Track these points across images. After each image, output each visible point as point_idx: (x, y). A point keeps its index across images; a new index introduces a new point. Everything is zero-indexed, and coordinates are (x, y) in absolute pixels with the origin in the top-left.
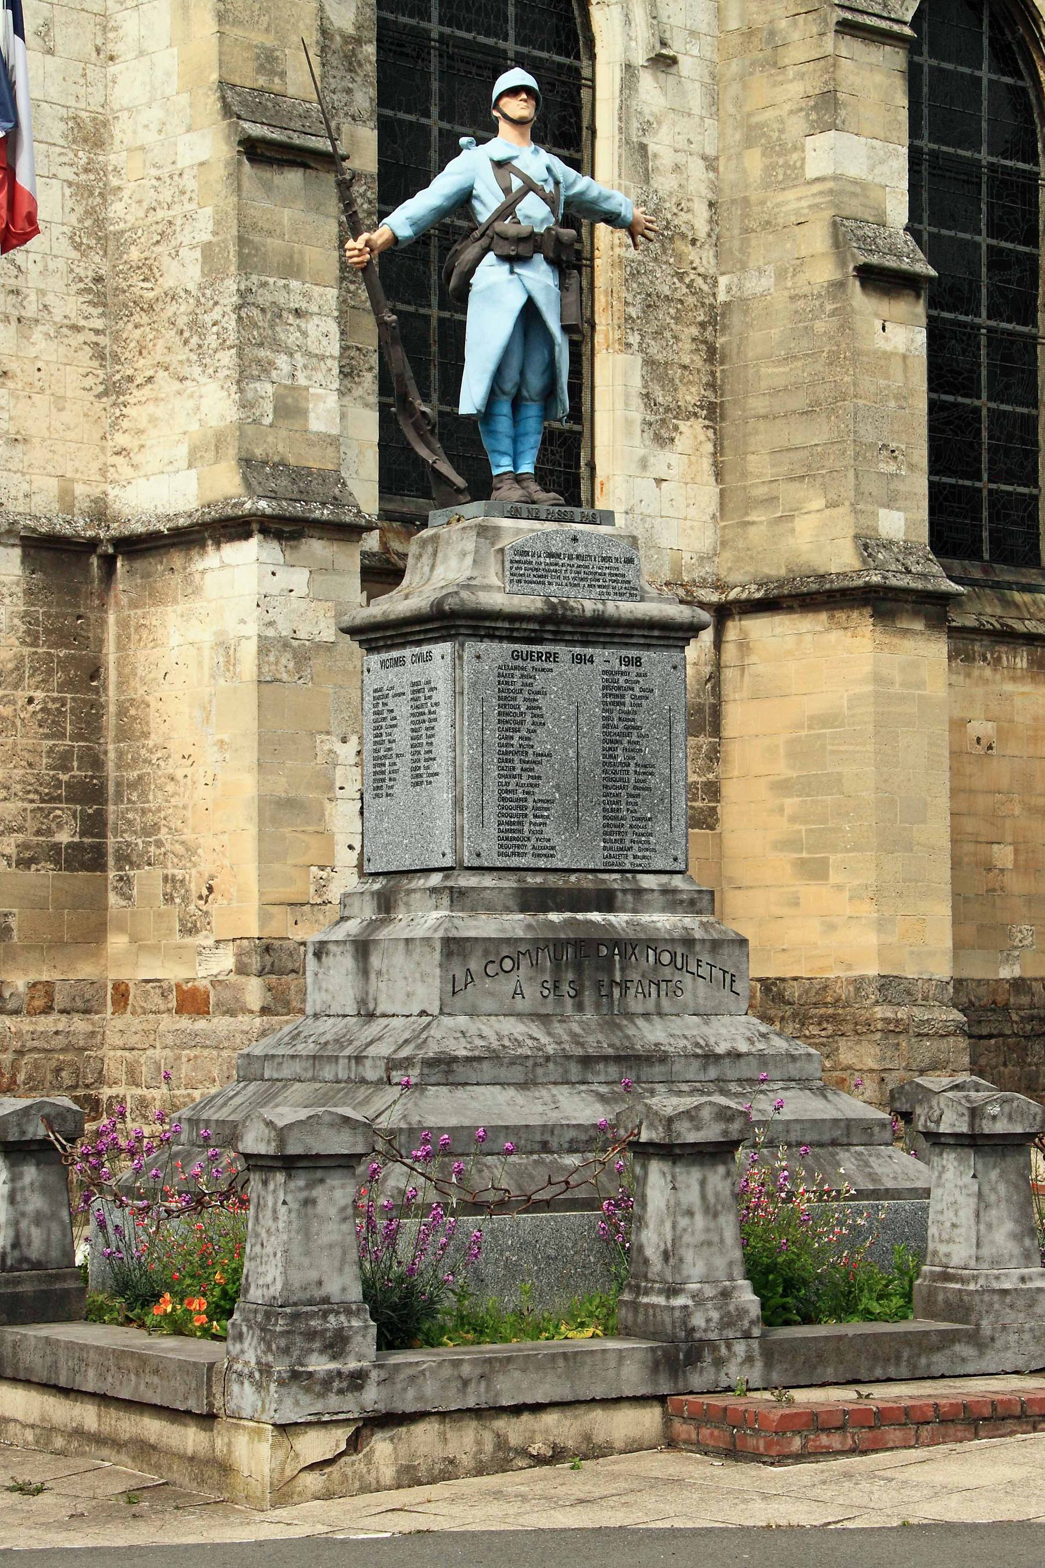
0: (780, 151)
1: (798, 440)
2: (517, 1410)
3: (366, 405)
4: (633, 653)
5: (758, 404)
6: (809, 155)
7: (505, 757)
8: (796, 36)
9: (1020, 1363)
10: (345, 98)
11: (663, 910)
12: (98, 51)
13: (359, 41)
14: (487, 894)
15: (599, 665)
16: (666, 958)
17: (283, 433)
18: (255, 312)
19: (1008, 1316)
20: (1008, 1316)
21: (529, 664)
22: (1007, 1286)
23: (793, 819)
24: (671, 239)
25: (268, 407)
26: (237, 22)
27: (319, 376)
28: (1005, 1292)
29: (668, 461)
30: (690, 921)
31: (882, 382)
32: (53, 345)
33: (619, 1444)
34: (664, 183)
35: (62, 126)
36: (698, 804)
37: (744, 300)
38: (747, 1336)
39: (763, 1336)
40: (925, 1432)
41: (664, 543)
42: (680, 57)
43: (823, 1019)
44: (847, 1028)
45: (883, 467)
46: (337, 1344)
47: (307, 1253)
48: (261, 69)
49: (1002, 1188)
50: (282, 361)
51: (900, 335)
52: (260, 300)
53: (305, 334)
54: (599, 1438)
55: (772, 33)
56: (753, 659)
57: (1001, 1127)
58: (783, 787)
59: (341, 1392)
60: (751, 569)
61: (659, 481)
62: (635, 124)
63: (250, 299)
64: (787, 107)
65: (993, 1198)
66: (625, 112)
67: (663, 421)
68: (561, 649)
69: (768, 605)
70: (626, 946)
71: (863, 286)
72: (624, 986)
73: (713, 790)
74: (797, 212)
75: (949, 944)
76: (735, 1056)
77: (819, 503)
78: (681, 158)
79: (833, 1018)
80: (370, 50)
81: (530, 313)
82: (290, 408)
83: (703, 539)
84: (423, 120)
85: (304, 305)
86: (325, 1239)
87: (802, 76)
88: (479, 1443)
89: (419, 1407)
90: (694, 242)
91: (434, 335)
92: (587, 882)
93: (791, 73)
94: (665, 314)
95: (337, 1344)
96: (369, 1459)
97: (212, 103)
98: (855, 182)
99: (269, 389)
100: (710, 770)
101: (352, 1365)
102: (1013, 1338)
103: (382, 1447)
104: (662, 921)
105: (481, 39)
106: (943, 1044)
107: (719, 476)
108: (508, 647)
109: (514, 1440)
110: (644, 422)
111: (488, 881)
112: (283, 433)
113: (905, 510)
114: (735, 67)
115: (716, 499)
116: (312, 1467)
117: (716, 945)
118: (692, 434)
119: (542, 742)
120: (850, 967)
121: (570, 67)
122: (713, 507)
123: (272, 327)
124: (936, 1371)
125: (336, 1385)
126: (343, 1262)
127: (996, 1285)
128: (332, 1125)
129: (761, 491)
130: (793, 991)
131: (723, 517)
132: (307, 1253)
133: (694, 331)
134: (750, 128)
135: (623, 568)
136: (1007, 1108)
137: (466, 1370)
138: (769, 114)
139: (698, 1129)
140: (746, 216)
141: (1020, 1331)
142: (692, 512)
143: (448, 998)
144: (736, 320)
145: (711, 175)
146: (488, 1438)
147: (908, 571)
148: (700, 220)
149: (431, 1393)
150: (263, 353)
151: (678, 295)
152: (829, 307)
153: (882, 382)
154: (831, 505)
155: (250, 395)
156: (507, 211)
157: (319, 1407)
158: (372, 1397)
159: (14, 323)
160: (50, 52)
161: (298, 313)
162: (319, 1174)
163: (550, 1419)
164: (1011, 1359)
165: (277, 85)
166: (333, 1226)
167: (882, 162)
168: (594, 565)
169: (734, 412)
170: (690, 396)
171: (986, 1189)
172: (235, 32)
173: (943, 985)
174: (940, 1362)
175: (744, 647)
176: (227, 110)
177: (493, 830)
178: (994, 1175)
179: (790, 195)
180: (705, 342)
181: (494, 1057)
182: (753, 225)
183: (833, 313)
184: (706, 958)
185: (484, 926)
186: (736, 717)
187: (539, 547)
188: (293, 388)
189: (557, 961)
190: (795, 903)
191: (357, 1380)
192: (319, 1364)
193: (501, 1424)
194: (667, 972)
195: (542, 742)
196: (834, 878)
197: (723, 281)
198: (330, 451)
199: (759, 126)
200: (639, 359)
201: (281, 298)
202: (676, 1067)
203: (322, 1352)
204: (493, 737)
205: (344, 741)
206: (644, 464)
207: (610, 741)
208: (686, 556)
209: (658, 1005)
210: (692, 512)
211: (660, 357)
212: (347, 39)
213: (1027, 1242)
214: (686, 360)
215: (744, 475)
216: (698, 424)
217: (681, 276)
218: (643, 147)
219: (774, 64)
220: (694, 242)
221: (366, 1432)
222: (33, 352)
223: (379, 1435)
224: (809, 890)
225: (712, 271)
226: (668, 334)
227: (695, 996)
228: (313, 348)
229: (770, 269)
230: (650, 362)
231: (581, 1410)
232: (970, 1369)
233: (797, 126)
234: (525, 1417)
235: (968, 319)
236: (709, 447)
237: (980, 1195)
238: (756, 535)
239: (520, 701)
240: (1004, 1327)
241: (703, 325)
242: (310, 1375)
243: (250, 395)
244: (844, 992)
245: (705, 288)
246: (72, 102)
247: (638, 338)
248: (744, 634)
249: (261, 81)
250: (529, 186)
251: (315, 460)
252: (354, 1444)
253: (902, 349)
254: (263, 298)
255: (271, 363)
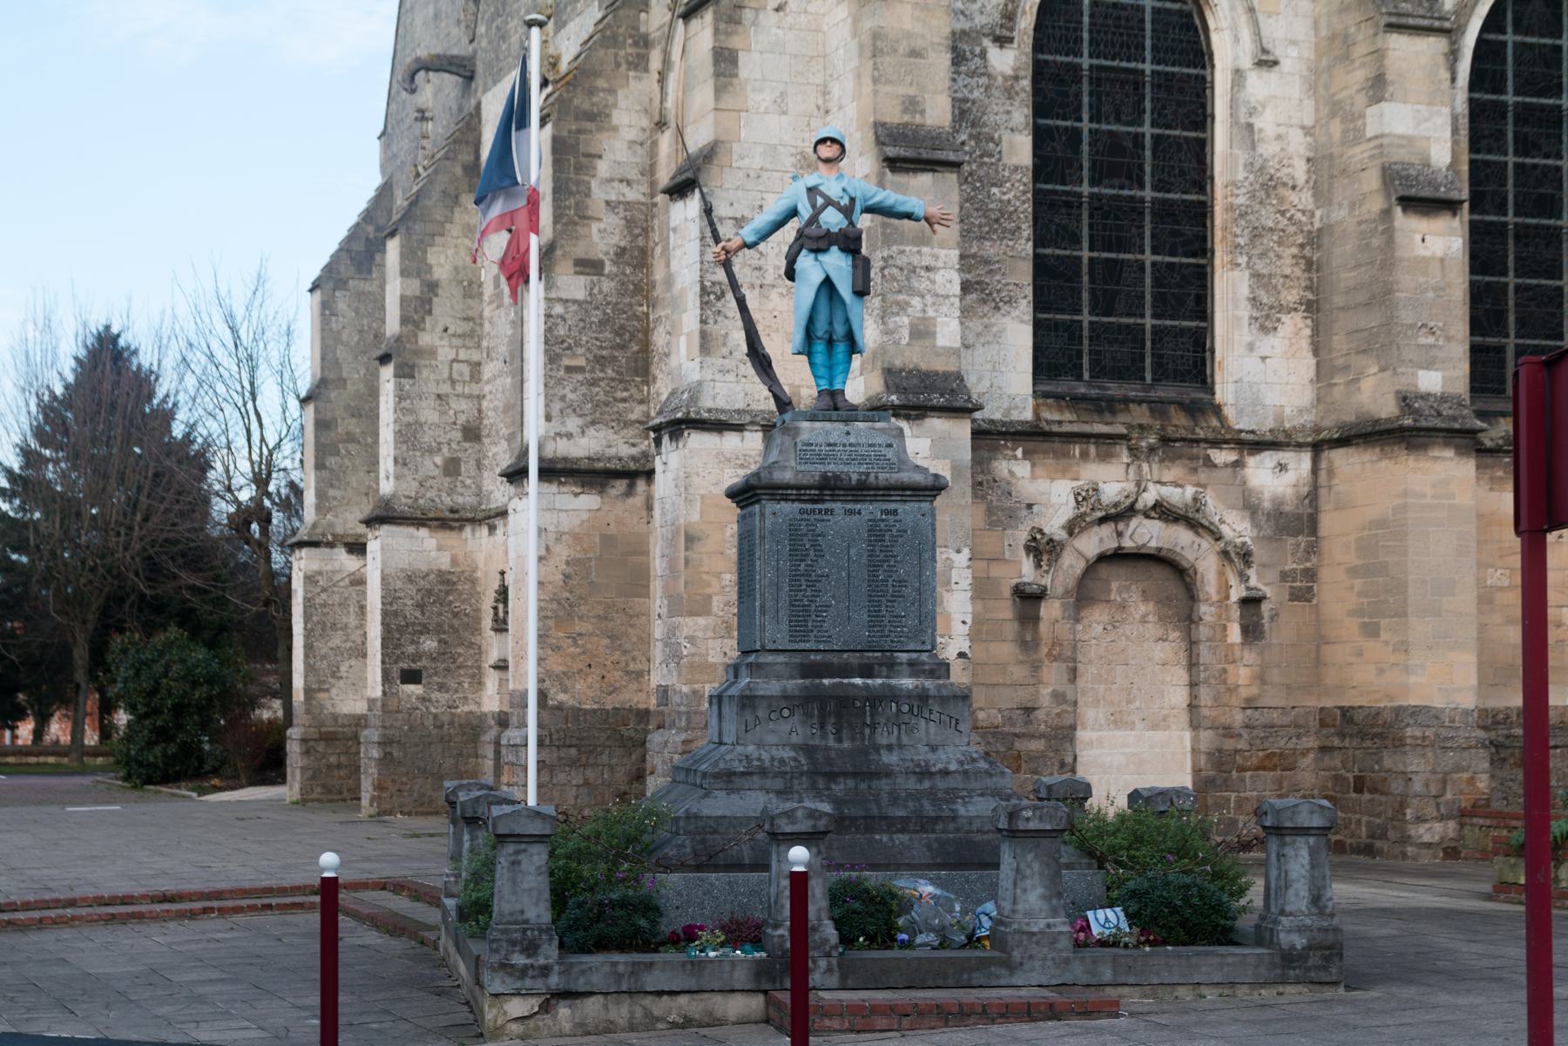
0: (1352, 120)
1: (1363, 324)
2: (660, 993)
3: (1022, 322)
4: (892, 506)
5: (1339, 300)
6: (1369, 120)
7: (794, 579)
8: (1360, 37)
9: (1044, 981)
10: (1005, 117)
11: (910, 676)
12: (818, 108)
13: (1016, 78)
14: (778, 668)
15: (865, 515)
16: (905, 708)
17: (917, 349)
18: (895, 271)
19: (1034, 950)
20: (1034, 950)
21: (812, 517)
22: (1035, 929)
23: (1359, 594)
24: (1275, 187)
25: (905, 333)
26: (888, 82)
27: (944, 309)
28: (1033, 934)
29: (1273, 345)
30: (929, 683)
31: (1422, 280)
32: (785, 301)
33: (732, 1019)
34: (1268, 149)
35: (793, 159)
36: (1298, 584)
37: (1330, 226)
38: (828, 955)
39: (841, 954)
40: (906, 1021)
41: (1268, 402)
42: (1282, 60)
43: (1375, 736)
44: (1388, 742)
45: (1422, 340)
46: (531, 949)
47: (514, 893)
48: (905, 111)
49: (1036, 866)
50: (916, 302)
51: (1441, 244)
52: (899, 263)
53: (933, 282)
54: (719, 1014)
55: (1346, 36)
56: (1336, 481)
57: (1032, 825)
58: (1353, 572)
59: (533, 977)
60: (1334, 417)
61: (1264, 358)
62: (1243, 110)
63: (891, 262)
64: (1355, 88)
65: (1028, 872)
66: (1233, 104)
67: (1268, 316)
68: (837, 506)
69: (1344, 441)
70: (876, 699)
71: (1405, 210)
72: (873, 727)
73: (1311, 575)
74: (1361, 161)
75: (1474, 682)
76: (945, 773)
77: (1374, 369)
78: (1282, 130)
79: (1381, 736)
80: (1026, 83)
81: (828, 283)
82: (923, 331)
83: (1306, 396)
84: (1076, 124)
85: (933, 263)
86: (526, 886)
87: (1363, 65)
88: (632, 1013)
89: (588, 989)
90: (1294, 188)
91: (1085, 269)
92: (854, 659)
93: (1357, 64)
94: (1269, 241)
95: (531, 949)
96: (555, 1018)
97: (871, 136)
98: (1401, 137)
99: (906, 320)
100: (1308, 560)
101: (542, 961)
102: (1037, 964)
103: (564, 1011)
104: (907, 683)
105: (1124, 64)
106: (1466, 754)
107: (1316, 352)
108: (797, 505)
109: (657, 1012)
110: (1251, 317)
111: (781, 658)
112: (917, 349)
113: (1443, 369)
114: (1324, 63)
115: (1313, 368)
116: (516, 1019)
117: (943, 700)
118: (1294, 326)
119: (822, 568)
120: (1392, 700)
121: (1197, 77)
122: (1311, 373)
123: (908, 280)
124: (974, 982)
125: (530, 972)
126: (538, 900)
127: (1025, 928)
128: (528, 817)
129: (1340, 362)
130: (1359, 717)
131: (1318, 381)
132: (514, 893)
133: (1294, 250)
134: (1334, 104)
135: (884, 451)
136: (1038, 813)
137: (621, 968)
138: (1345, 93)
139: (793, 823)
140: (1331, 166)
141: (1044, 959)
142: (1293, 379)
143: (742, 735)
144: (1326, 240)
145: (1309, 139)
146: (639, 1012)
147: (1439, 414)
148: (1300, 171)
149: (597, 980)
150: (901, 297)
151: (1280, 226)
152: (1381, 228)
153: (1422, 280)
154: (1382, 370)
155: (891, 326)
156: (814, 220)
157: (518, 985)
158: (554, 980)
159: (757, 290)
160: (784, 113)
161: (928, 269)
162: (523, 846)
163: (683, 1000)
164: (1036, 978)
165: (918, 119)
166: (531, 878)
167: (1427, 120)
168: (862, 450)
169: (1325, 307)
170: (1291, 296)
171: (1023, 866)
172: (885, 89)
173: (1466, 713)
174: (978, 978)
175: (1331, 473)
176: (879, 142)
177: (785, 626)
178: (1030, 857)
179: (1358, 149)
180: (1304, 257)
181: (763, 772)
182: (1336, 173)
183: (1383, 232)
184: (936, 708)
185: (772, 687)
186: (1329, 522)
187: (821, 440)
188: (924, 319)
189: (822, 709)
190: (1360, 654)
191: (545, 971)
192: (519, 959)
193: (648, 1001)
194: (906, 718)
195: (822, 568)
196: (1384, 636)
197: (1318, 213)
198: (953, 359)
199: (1339, 102)
200: (1247, 273)
201: (915, 260)
202: (899, 780)
203: (521, 952)
204: (785, 565)
205: (958, 551)
206: (1251, 347)
207: (874, 566)
208: (1288, 411)
209: (899, 738)
210: (1293, 379)
211: (1265, 271)
212: (1006, 78)
213: (1054, 901)
214: (1288, 271)
215: (1331, 350)
216: (1298, 317)
217: (1283, 213)
218: (1250, 126)
219: (1346, 58)
220: (1294, 188)
221: (553, 1002)
222: (770, 306)
223: (562, 1003)
224: (1369, 644)
225: (1309, 207)
226: (1271, 254)
227: (927, 732)
228: (941, 292)
229: (1346, 203)
230: (1256, 276)
231: (705, 996)
232: (1003, 982)
233: (1361, 100)
234: (665, 998)
235: (1552, 222)
236: (1308, 332)
237: (1018, 870)
238: (1338, 392)
239: (805, 540)
240: (1031, 957)
241: (1302, 246)
242: (512, 966)
243: (891, 326)
244: (1388, 716)
245: (1304, 219)
246: (799, 143)
247: (1245, 259)
248: (1330, 462)
249: (906, 118)
250: (829, 202)
251: (941, 365)
252: (545, 1008)
253: (1439, 253)
254: (901, 261)
255: (908, 304)
